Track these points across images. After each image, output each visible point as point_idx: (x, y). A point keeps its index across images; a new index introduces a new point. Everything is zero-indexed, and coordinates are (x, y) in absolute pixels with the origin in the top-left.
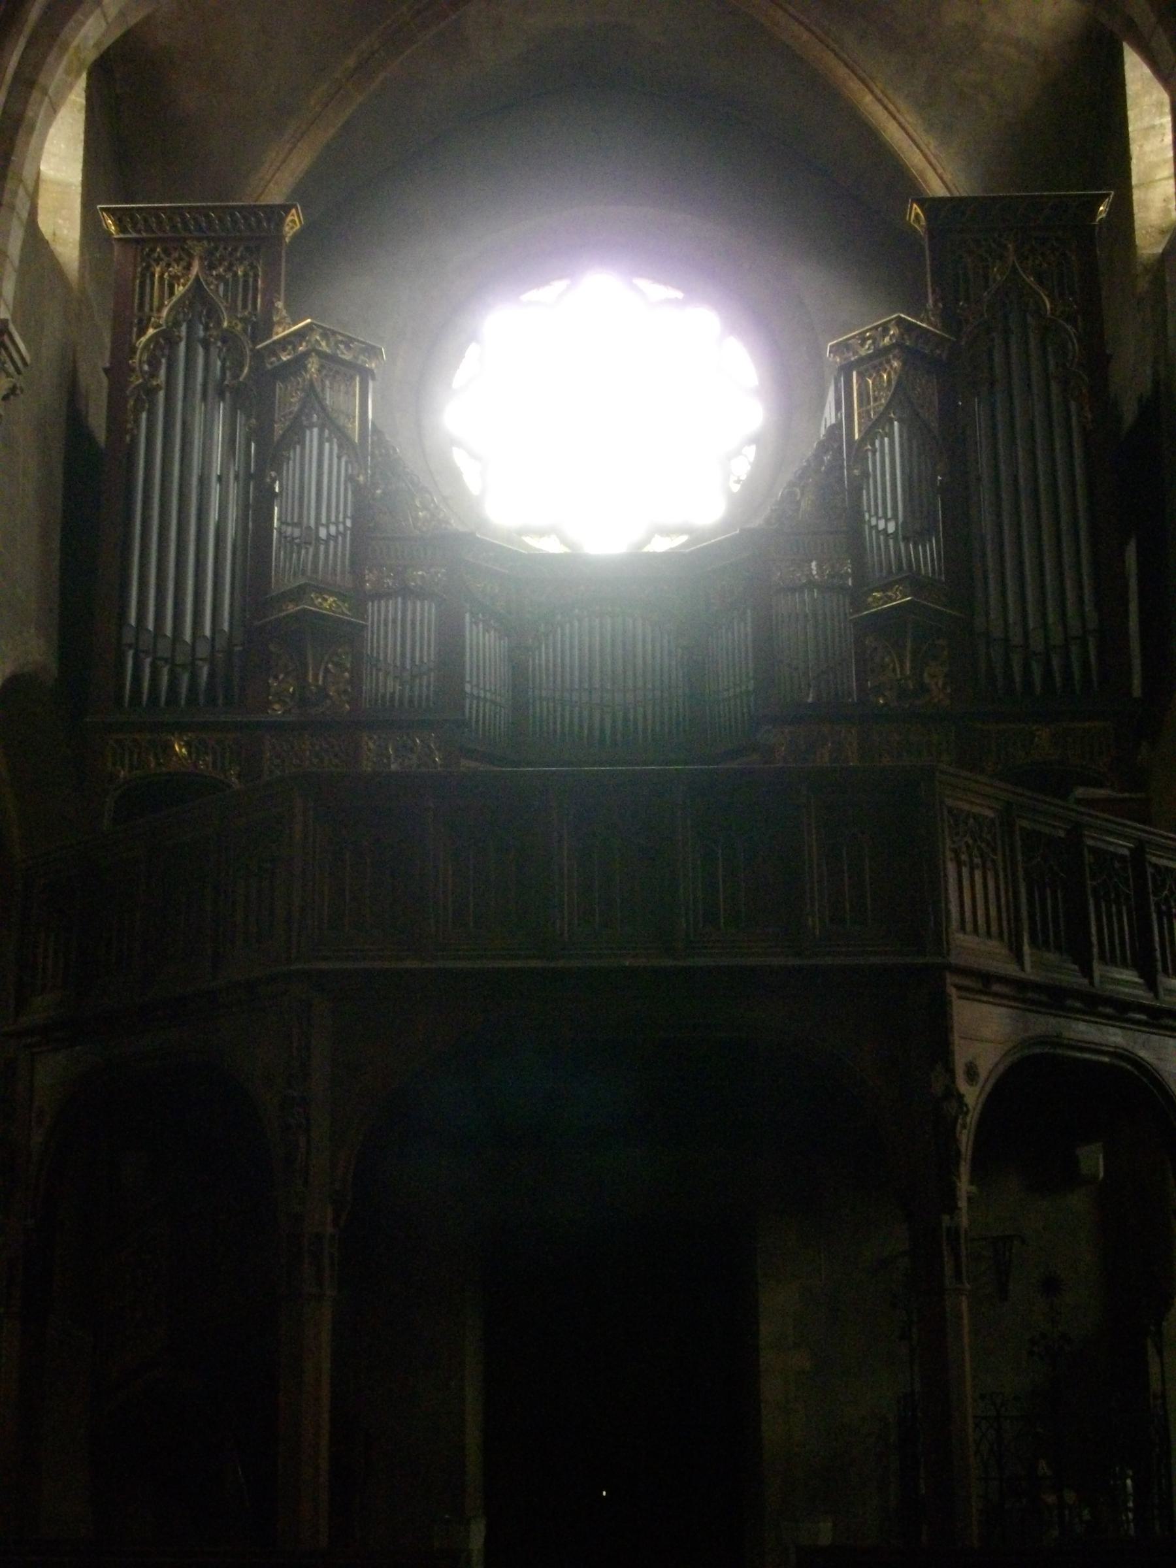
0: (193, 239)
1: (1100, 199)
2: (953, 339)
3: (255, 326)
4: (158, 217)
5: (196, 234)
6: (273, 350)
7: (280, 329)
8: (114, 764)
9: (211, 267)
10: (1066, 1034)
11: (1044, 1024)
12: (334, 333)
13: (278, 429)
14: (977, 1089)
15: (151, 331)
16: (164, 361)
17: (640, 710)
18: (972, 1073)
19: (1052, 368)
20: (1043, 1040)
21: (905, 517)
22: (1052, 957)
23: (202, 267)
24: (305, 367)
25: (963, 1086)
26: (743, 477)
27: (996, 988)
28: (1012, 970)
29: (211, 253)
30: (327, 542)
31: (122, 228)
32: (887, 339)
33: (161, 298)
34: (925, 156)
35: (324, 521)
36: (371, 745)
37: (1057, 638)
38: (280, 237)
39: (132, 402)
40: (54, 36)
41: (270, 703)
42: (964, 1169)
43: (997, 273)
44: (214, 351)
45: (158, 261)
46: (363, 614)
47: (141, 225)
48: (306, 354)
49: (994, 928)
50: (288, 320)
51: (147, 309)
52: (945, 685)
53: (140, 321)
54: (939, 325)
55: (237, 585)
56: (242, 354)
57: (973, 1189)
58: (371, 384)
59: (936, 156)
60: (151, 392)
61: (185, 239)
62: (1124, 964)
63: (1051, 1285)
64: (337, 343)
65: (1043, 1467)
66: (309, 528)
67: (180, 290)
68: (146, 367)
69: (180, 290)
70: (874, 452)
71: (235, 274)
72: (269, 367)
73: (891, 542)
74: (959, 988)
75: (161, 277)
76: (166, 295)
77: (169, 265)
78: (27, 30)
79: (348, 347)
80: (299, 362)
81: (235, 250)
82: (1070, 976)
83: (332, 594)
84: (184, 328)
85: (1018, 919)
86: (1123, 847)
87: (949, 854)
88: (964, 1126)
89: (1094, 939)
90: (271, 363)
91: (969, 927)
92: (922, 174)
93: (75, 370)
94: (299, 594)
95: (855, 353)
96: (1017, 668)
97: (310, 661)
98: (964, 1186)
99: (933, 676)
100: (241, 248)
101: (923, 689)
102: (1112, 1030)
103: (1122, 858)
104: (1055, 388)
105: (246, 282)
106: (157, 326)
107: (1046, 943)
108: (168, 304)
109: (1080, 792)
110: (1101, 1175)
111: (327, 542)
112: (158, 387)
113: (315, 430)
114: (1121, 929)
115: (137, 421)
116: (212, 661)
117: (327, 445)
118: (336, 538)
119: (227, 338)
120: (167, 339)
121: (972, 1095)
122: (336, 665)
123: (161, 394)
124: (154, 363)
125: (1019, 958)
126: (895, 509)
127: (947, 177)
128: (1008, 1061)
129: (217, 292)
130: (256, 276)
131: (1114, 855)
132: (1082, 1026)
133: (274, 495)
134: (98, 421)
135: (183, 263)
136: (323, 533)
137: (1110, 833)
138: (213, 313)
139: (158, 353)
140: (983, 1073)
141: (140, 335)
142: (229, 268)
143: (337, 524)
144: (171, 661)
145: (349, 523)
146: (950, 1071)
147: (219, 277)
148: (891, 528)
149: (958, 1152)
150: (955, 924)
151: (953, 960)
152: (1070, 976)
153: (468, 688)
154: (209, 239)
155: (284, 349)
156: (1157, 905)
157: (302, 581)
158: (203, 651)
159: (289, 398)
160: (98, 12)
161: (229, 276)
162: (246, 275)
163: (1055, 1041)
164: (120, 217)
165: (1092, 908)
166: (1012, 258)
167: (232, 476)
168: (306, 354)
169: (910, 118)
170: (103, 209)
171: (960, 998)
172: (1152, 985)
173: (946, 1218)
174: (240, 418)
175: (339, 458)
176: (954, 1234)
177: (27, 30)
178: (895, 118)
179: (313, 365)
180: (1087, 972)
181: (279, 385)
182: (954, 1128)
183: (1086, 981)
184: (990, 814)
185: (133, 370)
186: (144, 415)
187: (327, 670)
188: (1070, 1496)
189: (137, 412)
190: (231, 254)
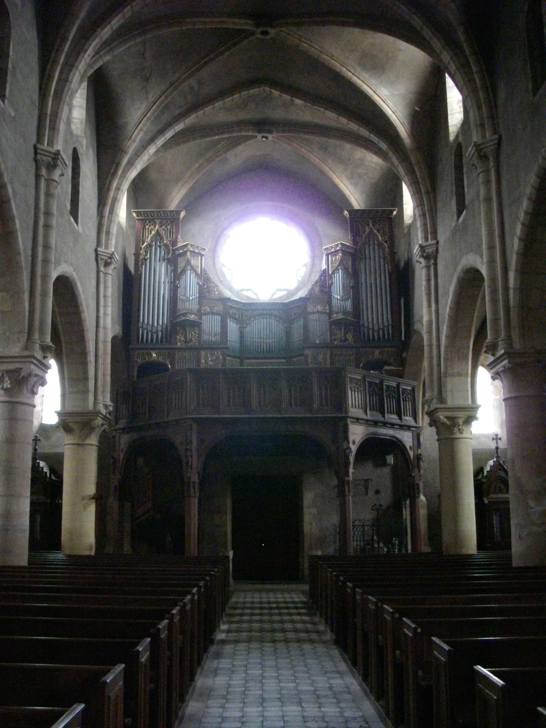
0: (156, 219)
1: (394, 210)
2: (355, 247)
3: (173, 242)
4: (147, 213)
5: (157, 218)
6: (177, 249)
7: (179, 244)
8: (137, 358)
9: (161, 226)
10: (378, 432)
11: (372, 429)
12: (194, 245)
13: (179, 270)
14: (355, 446)
15: (146, 244)
16: (149, 251)
17: (274, 344)
18: (354, 442)
19: (381, 255)
20: (372, 434)
21: (342, 294)
22: (374, 413)
23: (159, 226)
24: (186, 254)
25: (351, 445)
26: (302, 276)
27: (360, 421)
28: (364, 417)
29: (161, 223)
30: (192, 300)
31: (138, 216)
32: (338, 248)
33: (148, 234)
34: (350, 191)
35: (191, 295)
36: (203, 353)
37: (381, 326)
38: (179, 219)
39: (140, 263)
40: (124, 177)
41: (177, 343)
42: (351, 466)
43: (367, 230)
44: (162, 249)
45: (147, 224)
46: (201, 319)
47: (143, 215)
48: (186, 251)
49: (360, 406)
50: (182, 241)
51: (144, 237)
52: (352, 339)
53: (143, 241)
54: (352, 243)
55: (169, 309)
56: (169, 250)
57: (353, 471)
58: (203, 257)
59: (353, 192)
60: (146, 260)
61: (154, 219)
62: (394, 413)
63: (377, 492)
64: (195, 248)
65: (375, 538)
66: (187, 297)
67: (153, 233)
68: (144, 253)
69: (153, 233)
70: (334, 277)
71: (168, 228)
72: (177, 254)
73: (339, 301)
74: (350, 421)
75: (148, 229)
76: (149, 233)
77: (150, 226)
78: (118, 177)
79: (197, 249)
80: (185, 253)
81: (167, 222)
82: (379, 418)
83: (193, 314)
84: (154, 243)
85: (366, 404)
86: (394, 385)
87: (349, 388)
88: (351, 456)
89: (386, 408)
90: (177, 253)
91: (354, 406)
92: (349, 196)
93: (125, 254)
94: (185, 314)
95: (330, 251)
96: (371, 335)
97: (188, 333)
98: (351, 470)
99: (349, 336)
100: (169, 221)
101: (346, 340)
102: (390, 430)
103: (394, 387)
104: (382, 260)
105: (170, 231)
106: (148, 242)
107: (374, 410)
108: (150, 236)
109: (386, 368)
110: (392, 463)
111: (192, 300)
112: (148, 258)
113: (189, 271)
114: (393, 405)
115: (142, 267)
116: (162, 331)
117: (192, 275)
118: (194, 299)
119: (166, 245)
120: (150, 246)
121: (354, 448)
122: (194, 332)
123: (148, 260)
124: (146, 252)
125: (366, 414)
126: (340, 292)
127: (356, 197)
128: (364, 439)
129: (163, 233)
130: (173, 228)
131: (392, 387)
132: (382, 430)
133: (178, 287)
134: (132, 267)
135: (154, 225)
136: (191, 298)
137: (390, 381)
138: (162, 239)
139: (148, 249)
140: (357, 442)
141: (142, 245)
142: (166, 226)
143: (194, 295)
144: (151, 331)
145: (198, 295)
146: (349, 442)
147: (163, 229)
148: (339, 297)
149: (350, 462)
150: (350, 406)
151: (350, 415)
152: (379, 418)
153: (229, 339)
154: (161, 219)
155: (181, 249)
156: (403, 399)
157: (185, 311)
158: (160, 328)
159: (181, 263)
160: (135, 170)
161: (166, 229)
162: (170, 228)
163: (376, 434)
164: (137, 213)
165: (385, 400)
166: (371, 226)
167: (167, 282)
168: (186, 251)
169: (346, 182)
170: (134, 211)
171: (351, 424)
172: (400, 419)
173: (346, 478)
174: (169, 267)
175: (195, 278)
176: (348, 482)
177: (118, 177)
178: (342, 182)
179: (189, 254)
180: (384, 417)
181: (179, 258)
182: (349, 456)
183: (383, 419)
184: (359, 378)
185: (140, 254)
186: (144, 266)
187: (192, 334)
188: (381, 545)
189: (142, 264)
190: (166, 223)
